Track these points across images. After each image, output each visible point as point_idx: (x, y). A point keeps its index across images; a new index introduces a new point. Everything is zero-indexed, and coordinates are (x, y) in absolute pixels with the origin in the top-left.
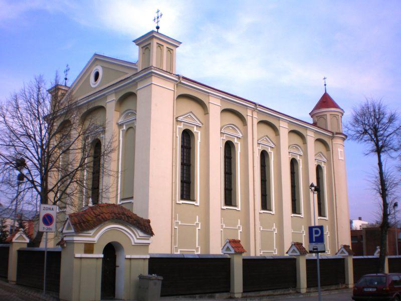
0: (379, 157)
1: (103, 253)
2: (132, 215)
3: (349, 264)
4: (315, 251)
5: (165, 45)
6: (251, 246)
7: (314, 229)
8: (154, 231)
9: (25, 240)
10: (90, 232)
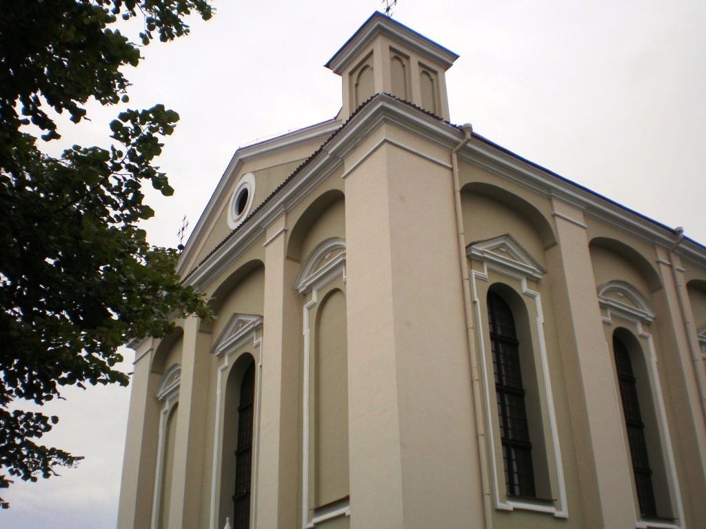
5: (414, 60)
6: (694, 413)
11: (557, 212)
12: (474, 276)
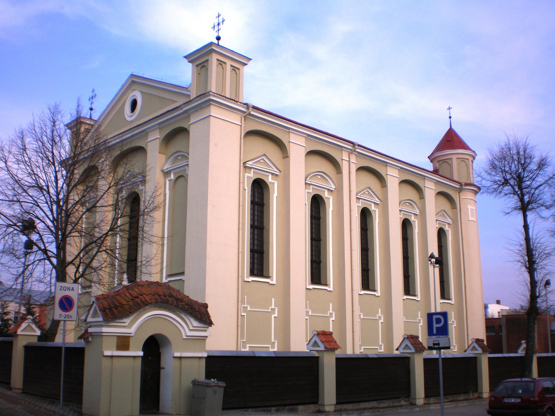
0: (525, 217)
4: (436, 346)
5: (229, 63)
7: (435, 317)
8: (213, 319)
9: (35, 332)
10: (125, 320)
11: (290, 141)
12: (246, 177)
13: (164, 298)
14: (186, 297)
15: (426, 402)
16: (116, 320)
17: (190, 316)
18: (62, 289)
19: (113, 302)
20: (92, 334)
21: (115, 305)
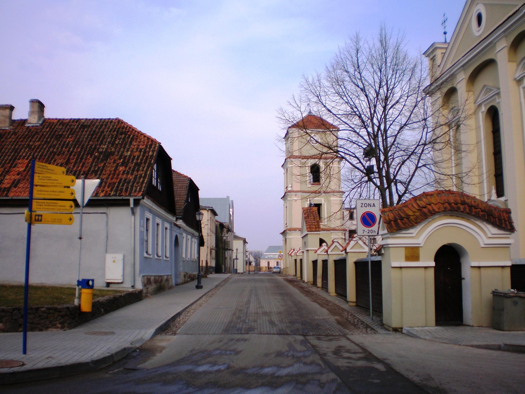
1: (435, 260)
2: (478, 204)
3: (466, 222)
8: (515, 225)
9: (364, 248)
10: (411, 231)
13: (455, 206)
14: (483, 203)
15: (203, 267)
16: (402, 231)
17: (486, 223)
18: (363, 205)
19: (399, 214)
20: (384, 246)
21: (401, 217)
